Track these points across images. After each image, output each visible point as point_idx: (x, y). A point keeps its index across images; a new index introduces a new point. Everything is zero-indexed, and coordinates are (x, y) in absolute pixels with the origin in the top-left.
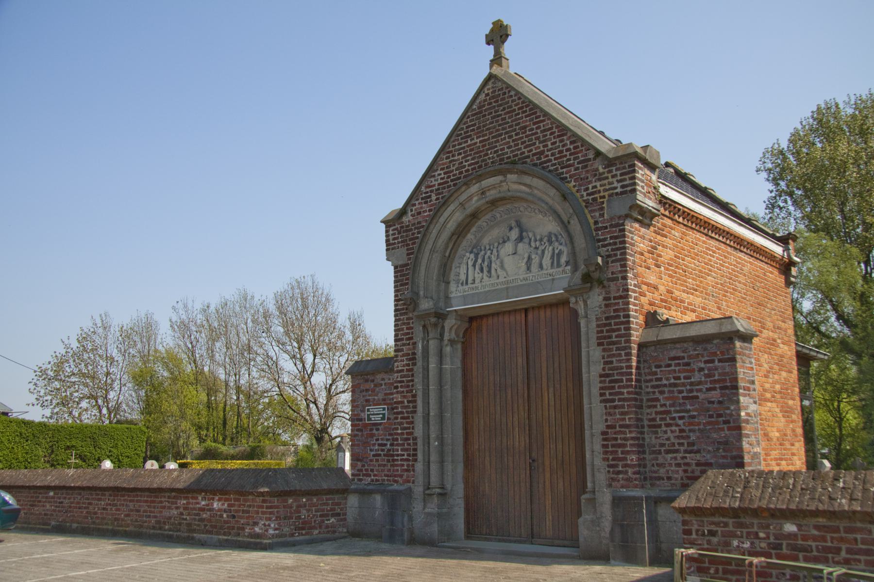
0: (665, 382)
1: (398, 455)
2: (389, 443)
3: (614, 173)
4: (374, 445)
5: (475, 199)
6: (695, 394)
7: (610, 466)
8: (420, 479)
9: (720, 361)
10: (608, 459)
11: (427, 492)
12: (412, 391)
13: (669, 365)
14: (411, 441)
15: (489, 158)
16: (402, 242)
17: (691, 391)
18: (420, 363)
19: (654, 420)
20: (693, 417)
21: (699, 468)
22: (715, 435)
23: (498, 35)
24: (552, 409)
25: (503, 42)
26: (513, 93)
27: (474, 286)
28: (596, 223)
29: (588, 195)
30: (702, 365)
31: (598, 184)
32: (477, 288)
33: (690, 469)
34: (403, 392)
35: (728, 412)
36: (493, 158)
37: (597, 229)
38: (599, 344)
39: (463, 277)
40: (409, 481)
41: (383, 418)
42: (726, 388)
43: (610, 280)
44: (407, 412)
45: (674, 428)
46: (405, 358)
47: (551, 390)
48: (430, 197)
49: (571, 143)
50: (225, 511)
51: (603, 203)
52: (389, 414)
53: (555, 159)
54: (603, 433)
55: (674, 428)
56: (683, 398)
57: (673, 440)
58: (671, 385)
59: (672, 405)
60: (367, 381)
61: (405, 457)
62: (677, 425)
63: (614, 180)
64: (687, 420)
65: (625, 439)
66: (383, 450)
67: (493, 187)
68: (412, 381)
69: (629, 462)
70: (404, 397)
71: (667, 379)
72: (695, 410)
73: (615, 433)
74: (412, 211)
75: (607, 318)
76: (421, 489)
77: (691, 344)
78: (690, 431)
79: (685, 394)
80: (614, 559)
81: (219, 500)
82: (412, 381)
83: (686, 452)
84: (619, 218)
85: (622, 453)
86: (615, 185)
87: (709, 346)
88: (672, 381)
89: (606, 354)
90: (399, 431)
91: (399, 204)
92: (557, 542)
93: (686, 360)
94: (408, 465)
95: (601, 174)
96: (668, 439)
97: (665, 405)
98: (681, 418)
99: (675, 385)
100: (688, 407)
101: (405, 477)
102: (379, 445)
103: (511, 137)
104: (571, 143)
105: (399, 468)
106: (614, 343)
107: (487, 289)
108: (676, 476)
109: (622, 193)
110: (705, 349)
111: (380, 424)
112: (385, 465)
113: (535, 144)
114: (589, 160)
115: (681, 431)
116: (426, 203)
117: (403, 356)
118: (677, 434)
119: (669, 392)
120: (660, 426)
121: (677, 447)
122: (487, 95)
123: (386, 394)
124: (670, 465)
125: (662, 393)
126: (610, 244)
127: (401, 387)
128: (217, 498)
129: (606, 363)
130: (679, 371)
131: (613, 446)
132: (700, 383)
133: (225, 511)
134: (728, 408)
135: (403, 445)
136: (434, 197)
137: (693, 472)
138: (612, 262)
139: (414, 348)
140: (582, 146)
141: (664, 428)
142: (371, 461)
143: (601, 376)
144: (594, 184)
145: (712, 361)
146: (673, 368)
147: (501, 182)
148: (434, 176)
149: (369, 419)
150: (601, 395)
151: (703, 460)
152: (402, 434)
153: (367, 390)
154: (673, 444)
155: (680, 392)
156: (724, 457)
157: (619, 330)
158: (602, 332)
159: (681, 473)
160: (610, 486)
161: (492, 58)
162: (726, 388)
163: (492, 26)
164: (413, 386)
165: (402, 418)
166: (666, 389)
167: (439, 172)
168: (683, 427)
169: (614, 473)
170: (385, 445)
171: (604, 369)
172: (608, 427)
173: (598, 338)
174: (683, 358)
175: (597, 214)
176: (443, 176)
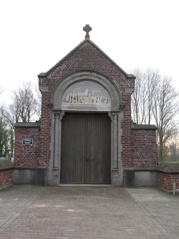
2: (33, 152)
3: (128, 81)
4: (26, 152)
6: (145, 143)
8: (52, 165)
9: (152, 136)
10: (123, 160)
11: (54, 169)
12: (49, 135)
13: (138, 135)
15: (85, 66)
16: (46, 84)
17: (144, 143)
18: (53, 126)
19: (133, 149)
23: (87, 29)
25: (89, 31)
27: (71, 103)
28: (122, 94)
29: (120, 85)
32: (73, 105)
33: (142, 162)
34: (45, 135)
35: (153, 148)
36: (86, 66)
37: (122, 96)
38: (122, 128)
39: (67, 100)
41: (31, 143)
42: (153, 142)
43: (126, 110)
45: (139, 152)
48: (60, 72)
52: (34, 142)
53: (109, 72)
54: (121, 152)
55: (139, 152)
56: (142, 144)
58: (138, 141)
59: (139, 146)
61: (45, 157)
62: (140, 151)
64: (142, 150)
65: (128, 154)
69: (129, 160)
70: (45, 137)
71: (138, 139)
73: (125, 153)
74: (51, 75)
75: (124, 121)
76: (52, 168)
82: (49, 132)
83: (142, 158)
84: (130, 94)
86: (129, 85)
90: (42, 148)
91: (46, 72)
94: (46, 160)
95: (124, 80)
97: (137, 146)
99: (139, 141)
100: (143, 147)
102: (28, 152)
104: (115, 69)
106: (126, 128)
108: (138, 164)
109: (130, 87)
115: (141, 153)
118: (140, 153)
119: (138, 142)
120: (135, 151)
122: (85, 46)
125: (136, 142)
126: (126, 101)
130: (141, 137)
131: (124, 156)
132: (146, 141)
136: (61, 73)
137: (143, 163)
138: (127, 105)
139: (50, 121)
140: (118, 71)
141: (136, 152)
143: (122, 137)
144: (122, 83)
145: (150, 136)
148: (62, 66)
150: (121, 142)
154: (138, 156)
157: (128, 124)
158: (123, 124)
161: (85, 35)
162: (153, 142)
164: (49, 133)
168: (141, 152)
169: (124, 163)
170: (32, 152)
171: (123, 135)
172: (123, 151)
173: (121, 126)
175: (123, 91)
176: (65, 66)
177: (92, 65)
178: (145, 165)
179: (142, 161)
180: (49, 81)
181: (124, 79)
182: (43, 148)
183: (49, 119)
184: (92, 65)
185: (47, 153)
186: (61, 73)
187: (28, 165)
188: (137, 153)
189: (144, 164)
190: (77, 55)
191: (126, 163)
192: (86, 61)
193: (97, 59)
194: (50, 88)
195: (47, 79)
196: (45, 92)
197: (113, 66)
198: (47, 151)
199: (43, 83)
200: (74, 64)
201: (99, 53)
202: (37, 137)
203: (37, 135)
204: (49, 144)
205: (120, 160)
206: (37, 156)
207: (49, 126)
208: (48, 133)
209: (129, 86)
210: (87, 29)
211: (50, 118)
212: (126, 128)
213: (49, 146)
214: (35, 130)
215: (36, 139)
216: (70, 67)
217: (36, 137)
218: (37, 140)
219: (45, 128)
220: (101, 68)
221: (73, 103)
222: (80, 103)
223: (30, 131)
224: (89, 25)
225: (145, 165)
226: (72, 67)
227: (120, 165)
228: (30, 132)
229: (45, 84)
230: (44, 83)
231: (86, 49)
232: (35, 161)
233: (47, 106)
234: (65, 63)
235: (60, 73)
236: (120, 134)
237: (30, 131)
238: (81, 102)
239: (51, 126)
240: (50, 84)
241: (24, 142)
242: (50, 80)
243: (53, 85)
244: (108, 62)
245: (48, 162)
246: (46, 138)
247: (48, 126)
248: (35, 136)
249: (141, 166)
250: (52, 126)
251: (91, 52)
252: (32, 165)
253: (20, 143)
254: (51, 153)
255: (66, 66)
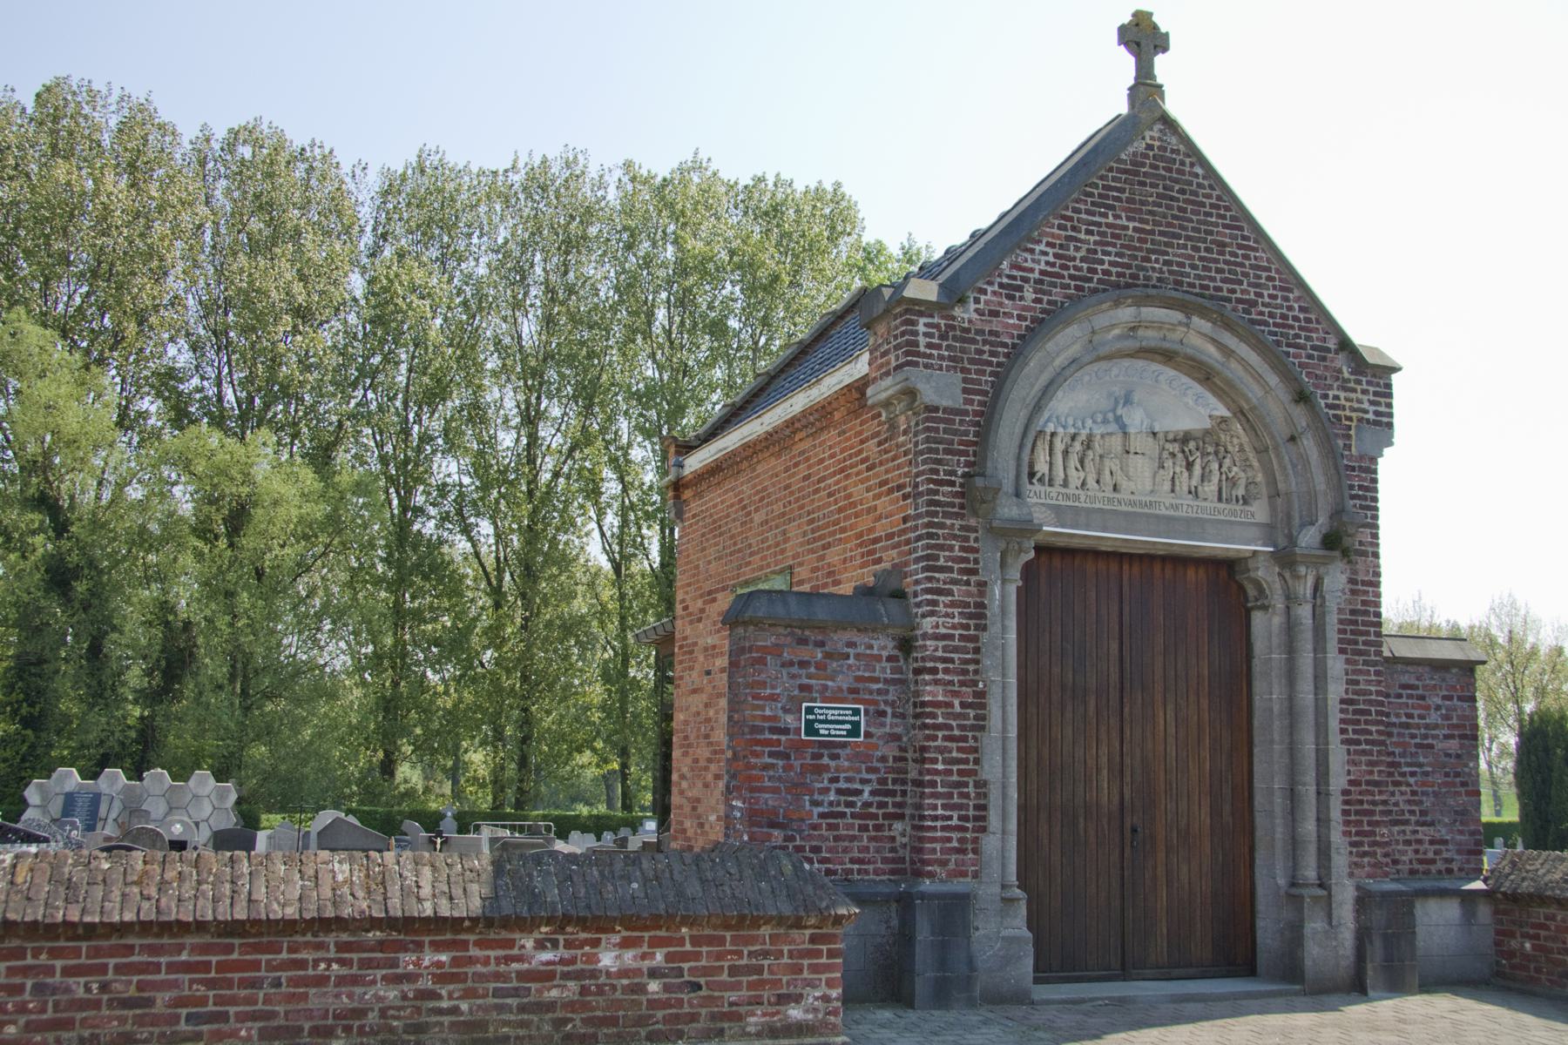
0: (1393, 719)
1: (935, 818)
2: (867, 789)
4: (826, 791)
5: (1117, 332)
6: (1430, 741)
7: (1352, 844)
11: (1294, 891)
12: (975, 683)
13: (1399, 696)
14: (971, 789)
15: (1153, 269)
16: (950, 358)
17: (1425, 737)
20: (1426, 774)
21: (1433, 848)
22: (1451, 802)
23: (1143, 38)
24: (1171, 740)
26: (1199, 170)
27: (1063, 490)
30: (1439, 702)
31: (1342, 395)
34: (951, 683)
38: (1342, 651)
40: (964, 874)
41: (854, 731)
44: (962, 728)
45: (1403, 788)
46: (956, 611)
47: (1170, 707)
48: (1020, 289)
49: (1301, 309)
50: (654, 973)
51: (1349, 428)
52: (867, 725)
54: (1345, 792)
55: (1403, 788)
57: (1402, 806)
59: (1402, 755)
60: (803, 641)
61: (955, 822)
62: (1409, 785)
63: (1365, 398)
65: (1374, 803)
66: (851, 804)
67: (1160, 325)
68: (977, 662)
70: (955, 694)
71: (1398, 716)
72: (1429, 765)
74: (977, 301)
75: (1353, 612)
76: (996, 889)
77: (1427, 669)
78: (1423, 793)
79: (1418, 740)
80: (1373, 988)
81: (626, 944)
82: (977, 662)
83: (1418, 823)
85: (1369, 823)
86: (1366, 406)
87: (1448, 676)
88: (1404, 719)
89: (1350, 667)
92: (1176, 972)
93: (1420, 692)
94: (961, 840)
96: (1396, 804)
98: (1413, 774)
99: (1407, 726)
100: (1421, 759)
101: (952, 866)
102: (839, 792)
103: (1197, 249)
104: (1301, 309)
105: (938, 846)
106: (1360, 653)
107: (1097, 506)
110: (1444, 680)
111: (844, 745)
112: (853, 838)
113: (1240, 283)
114: (1328, 350)
115: (1414, 793)
116: (1011, 297)
117: (953, 604)
121: (1407, 816)
123: (859, 679)
124: (1397, 842)
127: (946, 671)
128: (616, 939)
129: (1350, 682)
132: (1436, 726)
133: (654, 973)
134: (1466, 765)
135: (950, 795)
136: (1029, 294)
139: (982, 594)
142: (815, 827)
146: (1404, 700)
147: (1180, 323)
148: (1032, 251)
149: (811, 730)
150: (1343, 731)
151: (1438, 836)
152: (949, 772)
153: (803, 664)
155: (1413, 736)
156: (1461, 832)
159: (1411, 855)
160: (1351, 875)
163: (1163, 30)
164: (976, 672)
165: (946, 738)
166: (1395, 731)
167: (1042, 247)
170: (859, 792)
171: (1347, 692)
172: (1351, 782)
174: (1417, 688)
176: (1051, 259)
177: (1188, 270)
178: (1433, 862)
179: (1419, 842)
180: (964, 340)
181: (1345, 369)
182: (945, 762)
183: (973, 579)
184: (1188, 270)
185: (967, 796)
186: (1029, 294)
187: (835, 872)
188: (1397, 797)
189: (1430, 855)
190: (1107, 197)
191: (1365, 854)
192: (1159, 243)
193: (1211, 233)
194: (973, 381)
195: (953, 328)
196: (945, 410)
197: (1291, 291)
198: (966, 785)
199: (929, 346)
200: (1095, 252)
201: (1219, 198)
202: (887, 692)
203: (886, 681)
204: (975, 739)
205: (1337, 837)
206: (886, 816)
207: (977, 627)
208: (971, 668)
209: (1366, 412)
210: (1143, 38)
211: (974, 572)
212: (1360, 653)
213: (976, 750)
214: (871, 647)
215: (882, 707)
216: (1076, 268)
217: (879, 692)
218: (883, 714)
219: (951, 637)
220: (1233, 291)
221: (1071, 491)
222: (1109, 494)
223: (846, 650)
224: (1151, 14)
225: (1433, 862)
226: (1085, 266)
227: (1340, 861)
228: (848, 657)
229: (941, 358)
230: (938, 347)
231: (1156, 167)
232: (878, 851)
233: (956, 495)
234: (1048, 234)
235: (1021, 298)
236: (1336, 691)
237: (846, 650)
238: (1115, 488)
239: (984, 628)
240: (972, 361)
241: (814, 721)
242: (967, 330)
243: (989, 369)
244: (1268, 260)
245: (975, 851)
246: (957, 702)
247: (967, 627)
248: (875, 686)
249: (1416, 866)
250: (995, 629)
251: (1182, 192)
252: (859, 872)
253: (786, 731)
254: (992, 797)
255: (1056, 256)
